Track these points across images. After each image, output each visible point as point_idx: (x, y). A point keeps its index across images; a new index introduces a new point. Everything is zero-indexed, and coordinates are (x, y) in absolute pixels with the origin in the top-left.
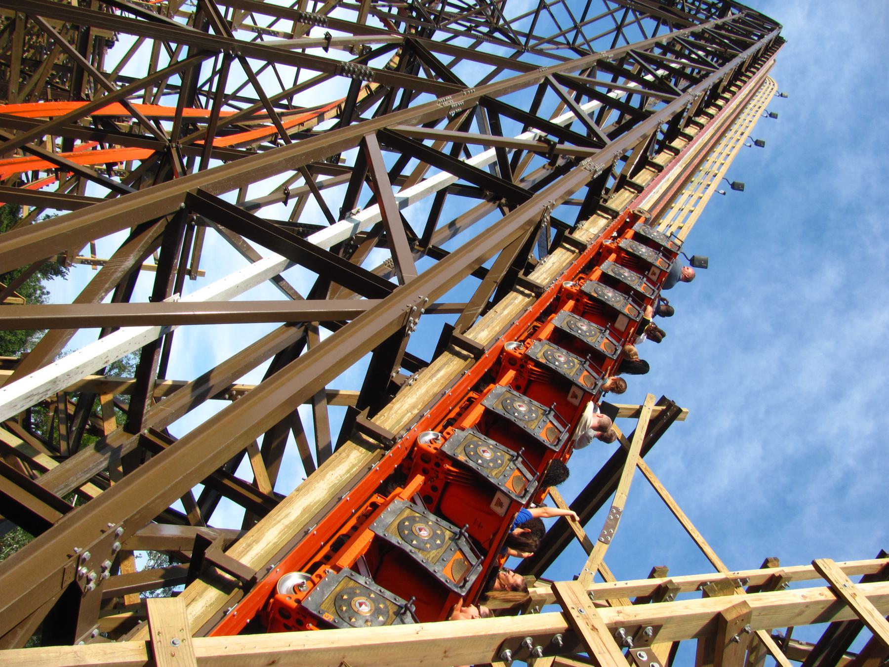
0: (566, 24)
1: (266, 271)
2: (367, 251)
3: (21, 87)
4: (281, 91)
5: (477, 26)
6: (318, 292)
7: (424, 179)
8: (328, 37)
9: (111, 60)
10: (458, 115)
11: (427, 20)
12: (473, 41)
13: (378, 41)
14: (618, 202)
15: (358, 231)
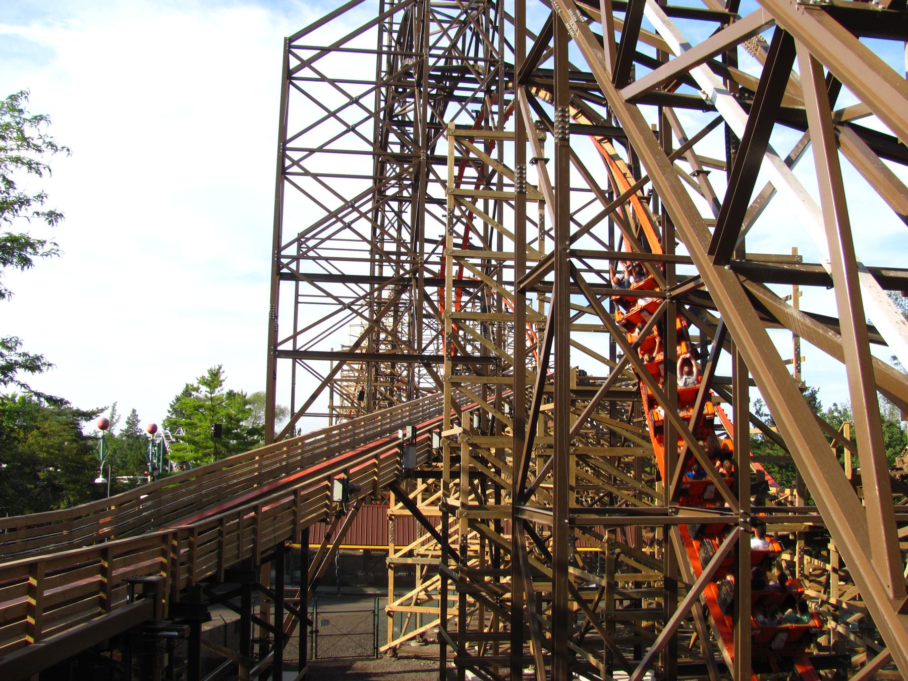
1: (784, 175)
2: (743, 76)
3: (637, 445)
4: (598, 201)
6: (797, 120)
7: (657, 32)
8: (535, 161)
9: (599, 370)
10: (584, 13)
11: (497, 73)
12: (506, 22)
13: (528, 112)
15: (724, 88)
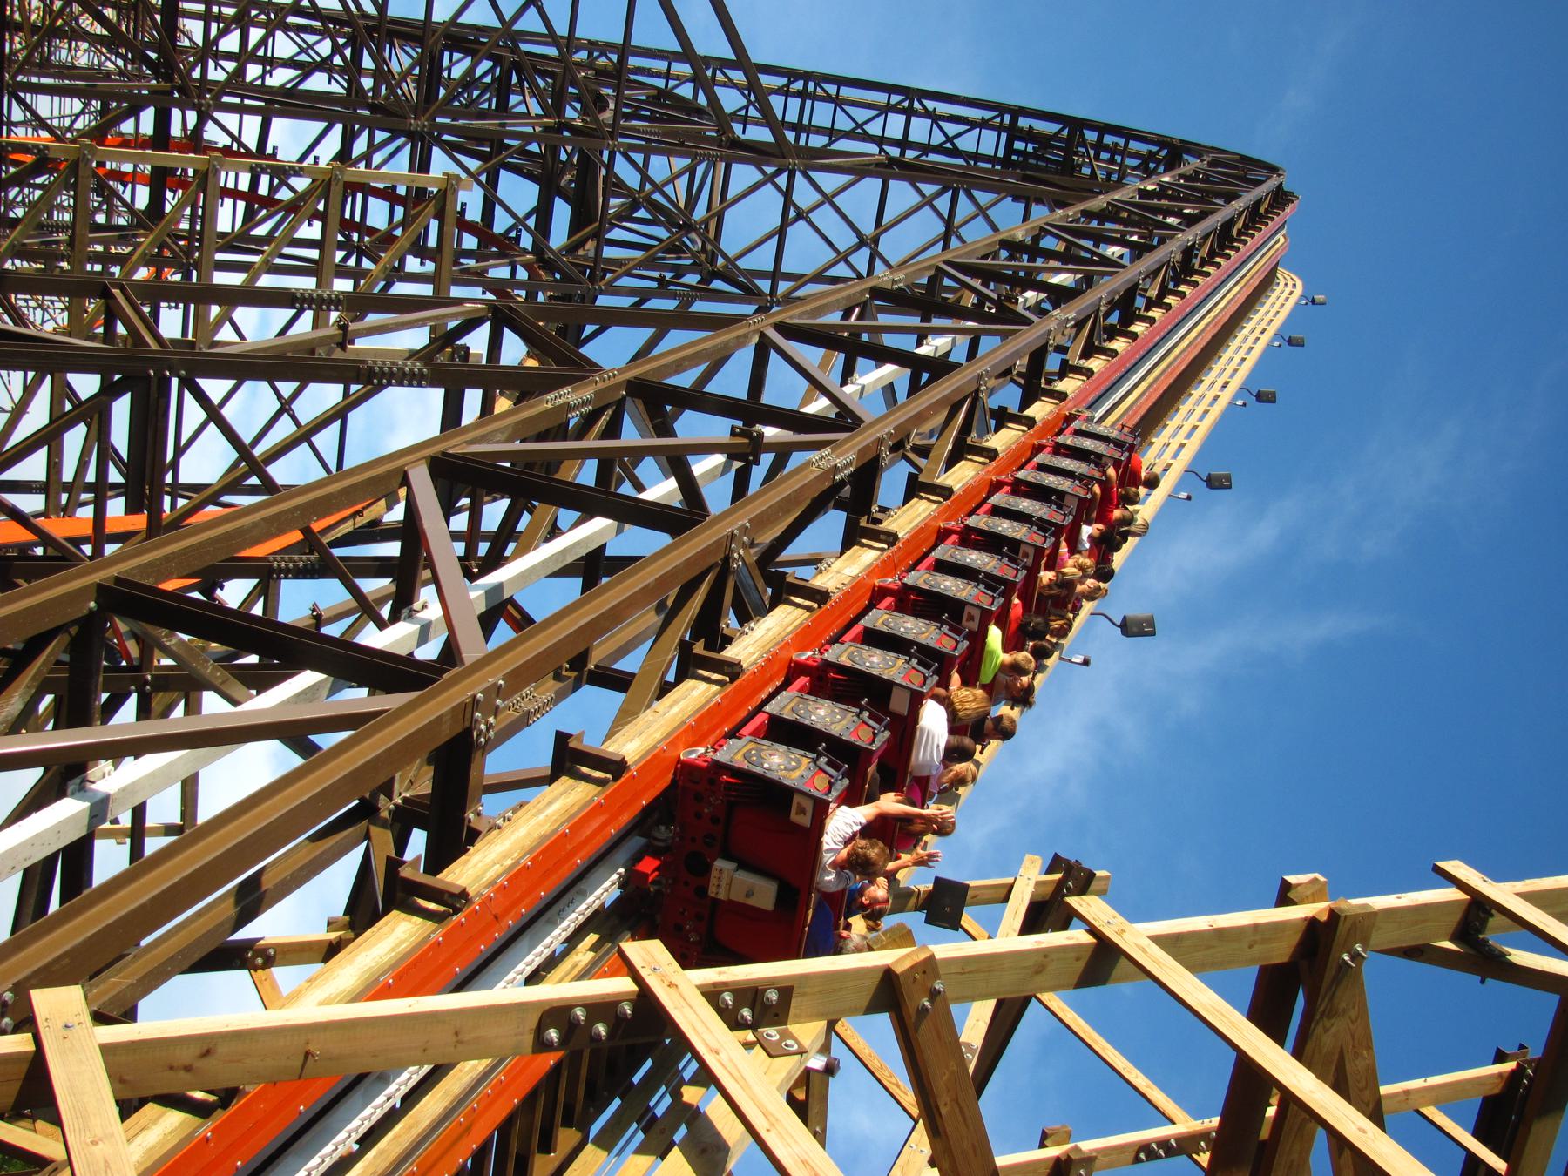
0: (845, 240)
5: (678, 276)
14: (902, 521)
